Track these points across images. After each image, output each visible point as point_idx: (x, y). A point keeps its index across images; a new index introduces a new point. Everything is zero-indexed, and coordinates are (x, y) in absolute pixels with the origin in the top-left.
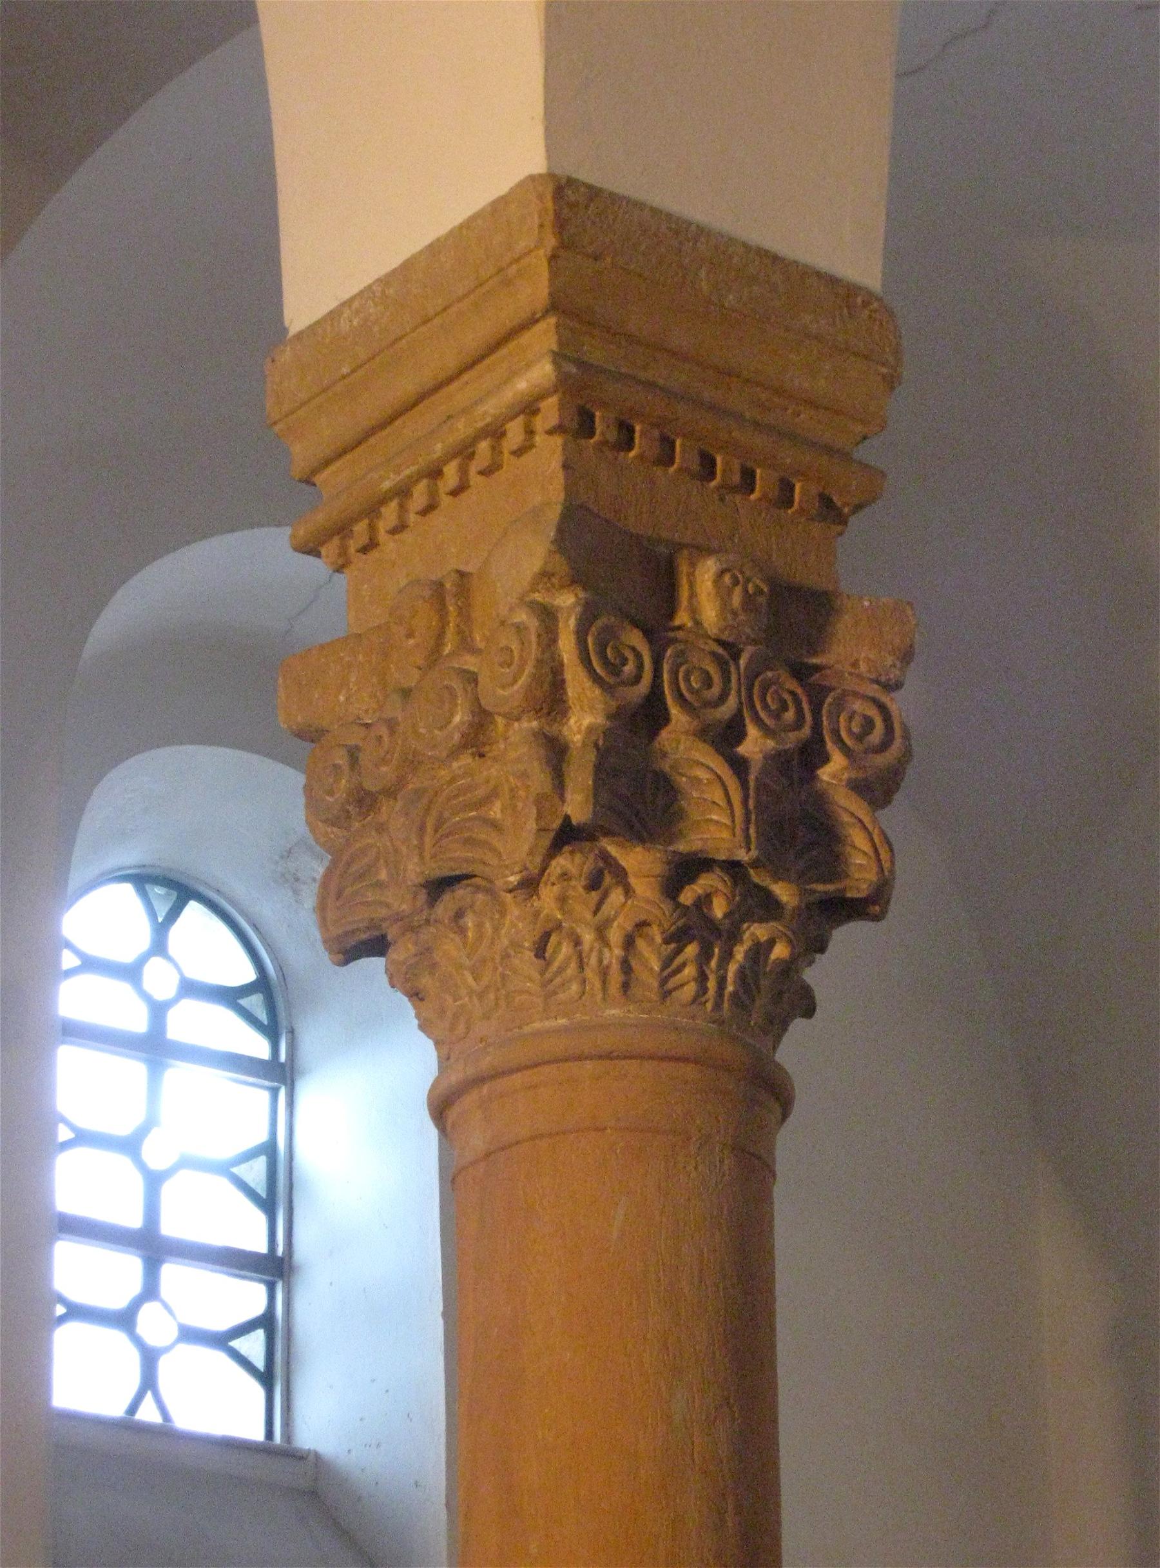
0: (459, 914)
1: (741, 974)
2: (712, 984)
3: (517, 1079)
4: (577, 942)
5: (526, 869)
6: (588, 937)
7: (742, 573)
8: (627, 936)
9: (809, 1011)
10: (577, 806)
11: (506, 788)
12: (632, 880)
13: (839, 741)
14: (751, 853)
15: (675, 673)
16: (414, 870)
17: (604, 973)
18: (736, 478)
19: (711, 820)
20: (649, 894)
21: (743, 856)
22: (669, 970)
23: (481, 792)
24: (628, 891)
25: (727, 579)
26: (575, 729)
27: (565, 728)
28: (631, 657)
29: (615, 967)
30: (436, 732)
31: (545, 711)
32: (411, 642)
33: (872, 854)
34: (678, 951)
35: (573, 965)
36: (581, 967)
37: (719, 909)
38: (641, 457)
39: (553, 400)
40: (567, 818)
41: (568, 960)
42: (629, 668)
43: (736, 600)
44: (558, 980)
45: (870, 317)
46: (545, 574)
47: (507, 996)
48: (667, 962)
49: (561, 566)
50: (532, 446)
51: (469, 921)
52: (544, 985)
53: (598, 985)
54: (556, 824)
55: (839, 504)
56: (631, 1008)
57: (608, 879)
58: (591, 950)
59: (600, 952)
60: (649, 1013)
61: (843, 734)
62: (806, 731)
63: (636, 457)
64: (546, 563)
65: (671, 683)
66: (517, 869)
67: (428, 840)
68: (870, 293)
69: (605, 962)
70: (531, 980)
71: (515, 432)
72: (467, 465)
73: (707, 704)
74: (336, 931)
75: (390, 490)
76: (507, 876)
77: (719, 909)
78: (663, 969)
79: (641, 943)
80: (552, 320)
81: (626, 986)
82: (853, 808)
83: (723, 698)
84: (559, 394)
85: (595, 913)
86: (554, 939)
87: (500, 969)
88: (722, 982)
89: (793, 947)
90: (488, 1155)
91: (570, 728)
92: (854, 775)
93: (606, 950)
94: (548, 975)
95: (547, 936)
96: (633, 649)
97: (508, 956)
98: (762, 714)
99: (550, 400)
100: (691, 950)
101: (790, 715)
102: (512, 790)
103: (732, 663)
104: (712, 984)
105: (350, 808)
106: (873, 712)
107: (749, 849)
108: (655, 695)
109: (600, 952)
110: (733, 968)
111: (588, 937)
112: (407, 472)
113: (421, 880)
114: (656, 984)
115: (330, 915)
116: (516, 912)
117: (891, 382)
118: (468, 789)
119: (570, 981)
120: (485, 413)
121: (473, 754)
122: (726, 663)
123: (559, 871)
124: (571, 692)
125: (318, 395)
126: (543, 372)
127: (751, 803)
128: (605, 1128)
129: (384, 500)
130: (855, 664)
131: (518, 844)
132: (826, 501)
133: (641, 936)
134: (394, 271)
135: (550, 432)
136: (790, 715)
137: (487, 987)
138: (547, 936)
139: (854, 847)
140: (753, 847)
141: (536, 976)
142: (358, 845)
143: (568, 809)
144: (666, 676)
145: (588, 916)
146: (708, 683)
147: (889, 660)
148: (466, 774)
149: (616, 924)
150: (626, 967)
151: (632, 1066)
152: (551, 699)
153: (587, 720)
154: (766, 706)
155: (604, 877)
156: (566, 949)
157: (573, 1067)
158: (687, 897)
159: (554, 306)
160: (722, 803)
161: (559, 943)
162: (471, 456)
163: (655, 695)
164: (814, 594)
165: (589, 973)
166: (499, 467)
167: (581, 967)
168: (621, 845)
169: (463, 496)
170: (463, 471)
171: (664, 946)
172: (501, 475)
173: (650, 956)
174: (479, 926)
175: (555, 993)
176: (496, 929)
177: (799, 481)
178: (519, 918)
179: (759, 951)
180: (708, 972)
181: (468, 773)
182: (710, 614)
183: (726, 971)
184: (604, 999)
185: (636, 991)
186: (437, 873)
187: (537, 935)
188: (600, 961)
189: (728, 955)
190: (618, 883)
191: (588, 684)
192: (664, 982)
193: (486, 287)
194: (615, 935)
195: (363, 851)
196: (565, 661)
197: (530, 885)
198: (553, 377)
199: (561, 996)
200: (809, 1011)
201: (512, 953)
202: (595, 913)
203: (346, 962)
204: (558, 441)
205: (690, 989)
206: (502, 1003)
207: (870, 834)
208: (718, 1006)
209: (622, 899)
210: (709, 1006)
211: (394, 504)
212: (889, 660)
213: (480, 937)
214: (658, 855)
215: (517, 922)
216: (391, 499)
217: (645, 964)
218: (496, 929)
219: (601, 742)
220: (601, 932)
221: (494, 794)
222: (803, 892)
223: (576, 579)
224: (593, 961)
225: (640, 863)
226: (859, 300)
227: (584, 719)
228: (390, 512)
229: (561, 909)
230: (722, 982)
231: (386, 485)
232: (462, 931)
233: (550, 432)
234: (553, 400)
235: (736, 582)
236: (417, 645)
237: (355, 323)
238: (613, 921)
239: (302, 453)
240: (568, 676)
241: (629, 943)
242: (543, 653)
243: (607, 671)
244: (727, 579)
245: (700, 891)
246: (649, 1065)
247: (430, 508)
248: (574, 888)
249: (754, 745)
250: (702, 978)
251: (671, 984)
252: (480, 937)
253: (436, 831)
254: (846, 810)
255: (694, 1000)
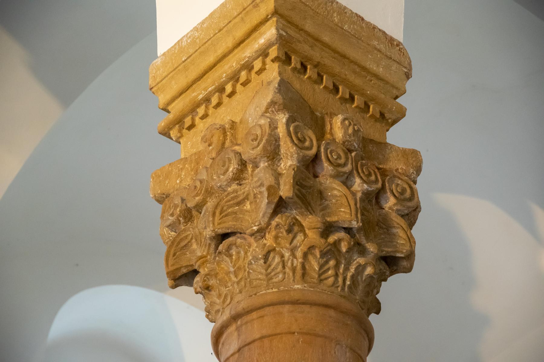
0: (229, 248)
1: (352, 277)
2: (340, 279)
3: (254, 315)
4: (282, 256)
5: (260, 224)
6: (287, 255)
7: (352, 121)
8: (304, 253)
9: (378, 312)
10: (286, 190)
11: (252, 195)
12: (307, 231)
13: (392, 192)
14: (359, 224)
15: (326, 150)
16: (208, 233)
17: (294, 270)
18: (347, 96)
19: (341, 211)
20: (315, 236)
21: (355, 224)
22: (322, 270)
23: (241, 198)
24: (305, 235)
25: (347, 122)
26: (283, 168)
27: (279, 168)
28: (308, 139)
29: (299, 267)
30: (222, 177)
31: (271, 157)
32: (211, 148)
33: (407, 240)
34: (327, 262)
35: (280, 266)
36: (284, 267)
37: (344, 248)
38: (309, 78)
39: (275, 47)
40: (281, 197)
41: (278, 264)
42: (307, 144)
43: (350, 131)
44: (273, 274)
45: (399, 50)
46: (273, 103)
47: (250, 281)
48: (321, 267)
49: (279, 98)
50: (265, 69)
51: (233, 252)
52: (267, 275)
53: (291, 274)
54: (276, 200)
55: (388, 118)
56: (306, 285)
57: (296, 228)
58: (289, 259)
59: (292, 261)
60: (313, 288)
61: (394, 191)
62: (380, 185)
63: (307, 78)
64: (274, 97)
65: (324, 155)
66: (257, 224)
67: (217, 219)
68: (400, 42)
69: (295, 265)
70: (261, 273)
71: (257, 65)
72: (236, 85)
73: (339, 165)
74: (171, 268)
75: (201, 100)
76: (252, 227)
77: (344, 248)
78: (320, 269)
79: (310, 257)
80: (275, 19)
81: (304, 275)
82: (398, 221)
83: (345, 165)
84: (278, 45)
85: (291, 244)
86: (272, 255)
87: (248, 269)
88: (344, 280)
89: (375, 269)
90: (239, 350)
91: (281, 168)
92: (399, 207)
93: (295, 260)
94: (269, 271)
95: (269, 252)
96: (310, 138)
97: (251, 264)
98: (362, 175)
99: (274, 48)
100: (332, 263)
101: (373, 178)
102: (255, 195)
103: (349, 154)
104: (340, 279)
105: (181, 219)
106: (406, 186)
107: (358, 222)
108: (317, 157)
109: (292, 261)
110: (349, 275)
111: (287, 255)
112: (210, 89)
113: (213, 234)
114: (317, 276)
115: (171, 262)
116: (256, 245)
117: (408, 76)
118: (236, 197)
119: (279, 273)
120: (245, 57)
121: (237, 184)
122: (347, 153)
123: (275, 224)
124: (283, 151)
125: (171, 72)
126: (273, 31)
127: (358, 205)
128: (294, 333)
129: (198, 105)
130: (398, 169)
131: (256, 212)
132: (382, 115)
133: (311, 254)
134: (206, 18)
135: (273, 61)
136: (373, 178)
137: (241, 279)
138: (269, 252)
139: (399, 236)
140: (359, 221)
141: (263, 271)
142: (184, 235)
143: (281, 193)
144: (322, 150)
145: (288, 245)
146: (339, 157)
147: (411, 171)
148: (233, 192)
149: (299, 249)
150: (303, 267)
151: (306, 308)
152: (273, 154)
153: (290, 163)
154: (363, 172)
155: (321, 113)
156: (277, 259)
157: (280, 308)
158: (332, 239)
159: (276, 12)
160: (346, 204)
161: (274, 258)
162: (237, 80)
163: (317, 157)
164: (380, 143)
165: (287, 270)
166: (250, 81)
167: (284, 267)
168: (302, 214)
169: (234, 97)
170: (234, 86)
171: (321, 259)
172: (250, 85)
173: (314, 264)
174: (238, 253)
175: (271, 279)
176: (246, 253)
177: (372, 104)
178: (256, 247)
179: (361, 269)
180: (339, 274)
181: (235, 191)
182: (339, 134)
183: (347, 275)
184: (294, 280)
185: (307, 278)
186: (220, 231)
187: (264, 252)
188: (292, 264)
189: (347, 269)
190: (301, 231)
191: (290, 145)
192: (320, 275)
193: (247, 10)
194: (299, 253)
195: (186, 237)
196: (281, 137)
197: (261, 232)
198: (275, 36)
199: (275, 280)
200: (378, 312)
201: (253, 263)
202: (291, 244)
203: (174, 287)
204: (276, 65)
205: (331, 280)
206: (248, 285)
207: (406, 233)
208: (343, 289)
209: (303, 237)
210: (339, 289)
211: (203, 107)
212: (411, 171)
213: (238, 258)
214: (319, 219)
215: (255, 249)
216: (202, 104)
217: (311, 266)
218: (246, 253)
219: (296, 169)
220: (293, 251)
221: (247, 198)
222: (380, 250)
223: (285, 107)
224: (289, 264)
225: (310, 221)
226: (395, 43)
227: (288, 162)
228: (201, 111)
229: (276, 242)
230: (344, 280)
231: (201, 97)
232: (230, 256)
233: (273, 61)
234: (275, 47)
235: (350, 124)
236: (213, 149)
237: (189, 41)
238: (299, 247)
239: (163, 99)
240: (282, 143)
241: (305, 255)
242: (272, 132)
243: (300, 142)
244: (347, 122)
245: (336, 238)
246: (314, 309)
247: (219, 105)
248: (282, 233)
249: (358, 185)
250: (336, 275)
251: (323, 277)
252: (238, 258)
253: (220, 214)
254: (396, 222)
255: (332, 286)
